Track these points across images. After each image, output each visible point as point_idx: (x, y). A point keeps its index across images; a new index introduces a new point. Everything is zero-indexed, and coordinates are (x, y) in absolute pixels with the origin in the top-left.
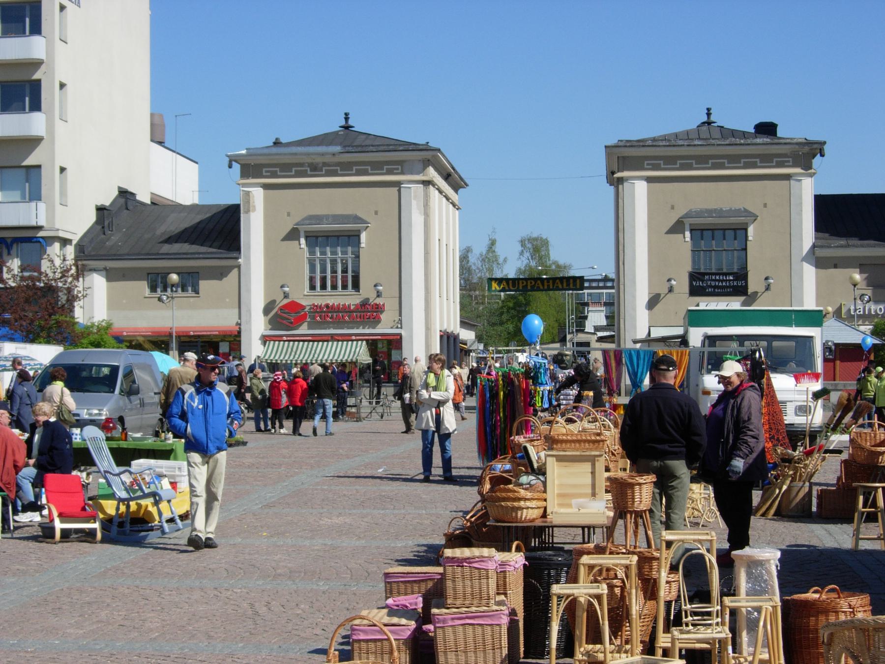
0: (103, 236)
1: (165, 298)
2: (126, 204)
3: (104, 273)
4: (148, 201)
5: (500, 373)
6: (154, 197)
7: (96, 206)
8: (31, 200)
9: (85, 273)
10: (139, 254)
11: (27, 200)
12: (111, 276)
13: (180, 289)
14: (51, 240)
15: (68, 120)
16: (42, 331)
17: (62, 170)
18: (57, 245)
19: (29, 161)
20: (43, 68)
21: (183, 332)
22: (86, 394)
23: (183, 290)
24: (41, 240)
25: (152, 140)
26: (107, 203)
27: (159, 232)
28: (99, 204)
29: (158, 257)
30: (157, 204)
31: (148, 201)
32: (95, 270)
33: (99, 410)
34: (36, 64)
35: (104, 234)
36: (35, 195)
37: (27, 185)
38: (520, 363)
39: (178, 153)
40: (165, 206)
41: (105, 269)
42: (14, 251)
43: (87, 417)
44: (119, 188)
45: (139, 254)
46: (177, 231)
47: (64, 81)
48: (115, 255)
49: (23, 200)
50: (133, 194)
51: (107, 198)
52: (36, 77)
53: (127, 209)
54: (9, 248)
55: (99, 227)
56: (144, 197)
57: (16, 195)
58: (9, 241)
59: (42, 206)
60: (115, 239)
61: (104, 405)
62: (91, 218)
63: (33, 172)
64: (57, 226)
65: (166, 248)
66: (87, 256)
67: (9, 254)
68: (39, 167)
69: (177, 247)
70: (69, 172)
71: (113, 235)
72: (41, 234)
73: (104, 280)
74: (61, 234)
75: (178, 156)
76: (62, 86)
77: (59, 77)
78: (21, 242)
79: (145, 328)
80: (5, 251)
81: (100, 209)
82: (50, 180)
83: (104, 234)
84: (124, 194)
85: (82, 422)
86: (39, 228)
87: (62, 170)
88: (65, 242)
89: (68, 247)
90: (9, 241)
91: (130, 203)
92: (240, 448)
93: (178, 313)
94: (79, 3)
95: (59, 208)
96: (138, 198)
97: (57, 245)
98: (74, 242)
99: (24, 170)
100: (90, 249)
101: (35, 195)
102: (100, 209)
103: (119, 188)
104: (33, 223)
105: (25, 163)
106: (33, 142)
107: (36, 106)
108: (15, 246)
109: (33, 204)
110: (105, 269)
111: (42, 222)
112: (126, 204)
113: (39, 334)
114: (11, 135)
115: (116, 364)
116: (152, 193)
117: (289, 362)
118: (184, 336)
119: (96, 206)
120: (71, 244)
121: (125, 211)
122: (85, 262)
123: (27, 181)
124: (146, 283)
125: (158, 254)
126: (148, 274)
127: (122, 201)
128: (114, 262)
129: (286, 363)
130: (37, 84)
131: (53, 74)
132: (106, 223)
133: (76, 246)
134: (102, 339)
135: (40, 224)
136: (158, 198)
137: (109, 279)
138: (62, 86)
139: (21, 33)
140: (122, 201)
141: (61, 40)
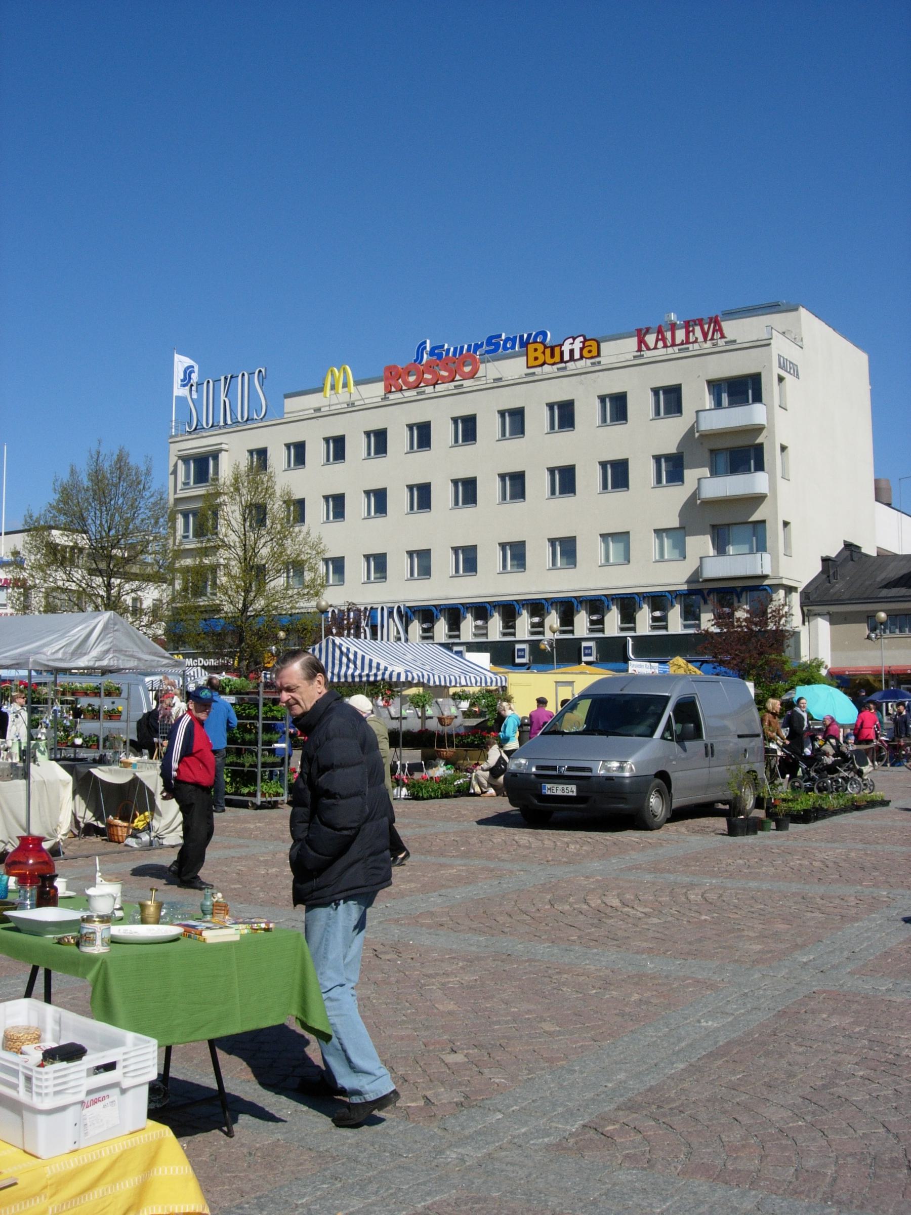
0: (829, 585)
1: (873, 636)
2: (852, 556)
3: (828, 617)
4: (875, 554)
5: (138, 616)
6: (880, 550)
7: (822, 557)
8: (757, 551)
9: (811, 618)
10: (859, 599)
11: (755, 551)
12: (834, 619)
13: (897, 630)
14: (776, 587)
15: (790, 479)
16: (752, 669)
17: (786, 524)
18: (782, 593)
19: (755, 517)
20: (765, 433)
21: (901, 670)
22: (610, 737)
23: (901, 631)
24: (767, 588)
25: (877, 500)
26: (833, 554)
27: (878, 579)
28: (824, 556)
29: (876, 600)
30: (884, 557)
31: (875, 554)
32: (819, 615)
33: (621, 762)
34: (758, 430)
35: (830, 582)
36: (761, 547)
37: (754, 539)
38: (372, 712)
39: (903, 513)
40: (887, 556)
41: (828, 613)
42: (743, 599)
43: (602, 772)
44: (845, 541)
45: (859, 599)
46: (897, 577)
47: (785, 444)
48: (838, 600)
49: (751, 552)
50: (859, 548)
51: (834, 550)
52: (758, 441)
53: (852, 560)
54: (739, 597)
55: (825, 576)
56: (870, 550)
57: (745, 548)
58: (739, 590)
59: (767, 557)
60: (839, 586)
61: (629, 755)
62: (818, 568)
63: (760, 526)
64: (781, 575)
65: (885, 593)
66: (812, 602)
67: (739, 602)
68: (764, 522)
69: (895, 592)
70: (792, 526)
71: (837, 583)
72: (767, 582)
73: (828, 623)
74: (785, 582)
75: (903, 515)
76: (783, 448)
77: (780, 439)
78: (750, 591)
79: (866, 667)
80: (735, 599)
81: (825, 560)
82: (775, 535)
83: (830, 582)
84: (849, 547)
85: (594, 779)
86: (765, 577)
87: (786, 524)
88: (790, 590)
89: (793, 594)
90: (739, 590)
91: (855, 555)
92: (878, 810)
93: (886, 653)
94: (798, 375)
95: (783, 559)
96: (863, 551)
97: (782, 593)
98: (800, 590)
99: (751, 526)
100: (815, 596)
101: (761, 547)
102: (825, 560)
103: (845, 541)
104: (759, 573)
105: (751, 520)
106: (759, 499)
107: (760, 467)
108: (744, 595)
109: (759, 555)
110: (828, 613)
111: (767, 571)
112: (852, 556)
113: (749, 672)
114: (738, 493)
115: (667, 694)
116: (878, 548)
117: (372, 679)
118: (903, 674)
119: (822, 557)
120: (796, 591)
121: (851, 562)
122: (810, 608)
123: (754, 536)
124: (866, 625)
125: (877, 598)
126: (868, 617)
127: (848, 553)
128: (840, 606)
129: (368, 681)
130: (760, 447)
131: (774, 437)
132: (831, 573)
133: (801, 593)
134: (812, 677)
135: (765, 573)
136: (882, 551)
137: (833, 622)
138: (783, 448)
139: (745, 402)
140: (848, 553)
141: (780, 406)
